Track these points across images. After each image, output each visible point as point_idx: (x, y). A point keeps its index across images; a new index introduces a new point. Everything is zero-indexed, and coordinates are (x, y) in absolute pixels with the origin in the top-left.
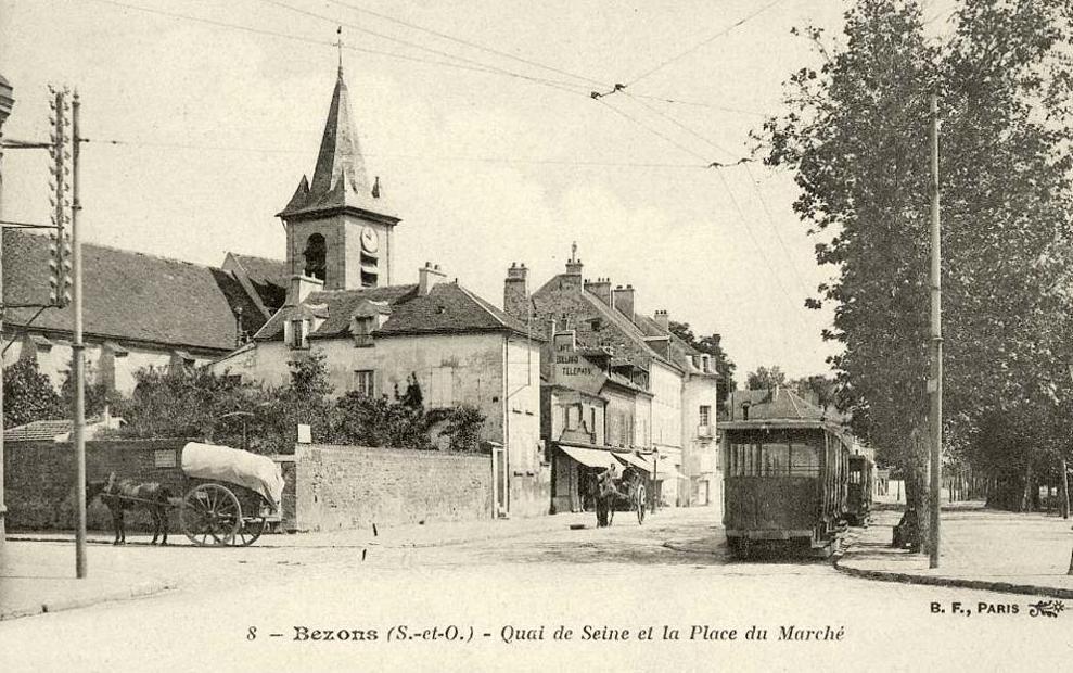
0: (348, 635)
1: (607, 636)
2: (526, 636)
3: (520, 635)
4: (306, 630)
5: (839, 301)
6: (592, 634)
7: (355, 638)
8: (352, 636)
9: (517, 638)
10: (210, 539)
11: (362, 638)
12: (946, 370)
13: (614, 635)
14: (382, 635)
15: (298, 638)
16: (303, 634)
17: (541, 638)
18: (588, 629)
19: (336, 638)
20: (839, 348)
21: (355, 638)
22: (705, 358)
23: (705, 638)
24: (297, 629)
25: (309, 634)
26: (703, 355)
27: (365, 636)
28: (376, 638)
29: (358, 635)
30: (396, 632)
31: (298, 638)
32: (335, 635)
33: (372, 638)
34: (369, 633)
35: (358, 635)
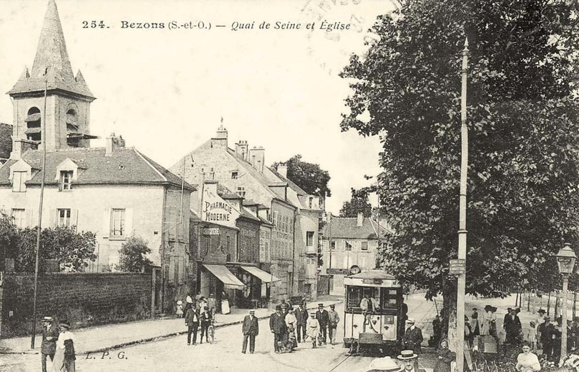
0: (149, 26)
1: (289, 27)
2: (244, 27)
3: (242, 26)
4: (127, 23)
5: (574, 253)
6: (281, 26)
7: (153, 27)
8: (151, 26)
9: (246, 28)
10: (330, 317)
11: (156, 27)
12: (39, 277)
13: (248, 26)
14: (166, 26)
15: (123, 27)
16: (125, 24)
17: (252, 28)
18: (278, 24)
19: (143, 27)
20: (521, 333)
21: (153, 27)
22: (311, 198)
23: (260, 28)
24: (123, 22)
25: (129, 25)
26: (309, 196)
27: (158, 26)
28: (164, 27)
29: (155, 26)
30: (171, 25)
31: (123, 27)
32: (142, 25)
33: (162, 24)
34: (160, 24)
35: (155, 26)
